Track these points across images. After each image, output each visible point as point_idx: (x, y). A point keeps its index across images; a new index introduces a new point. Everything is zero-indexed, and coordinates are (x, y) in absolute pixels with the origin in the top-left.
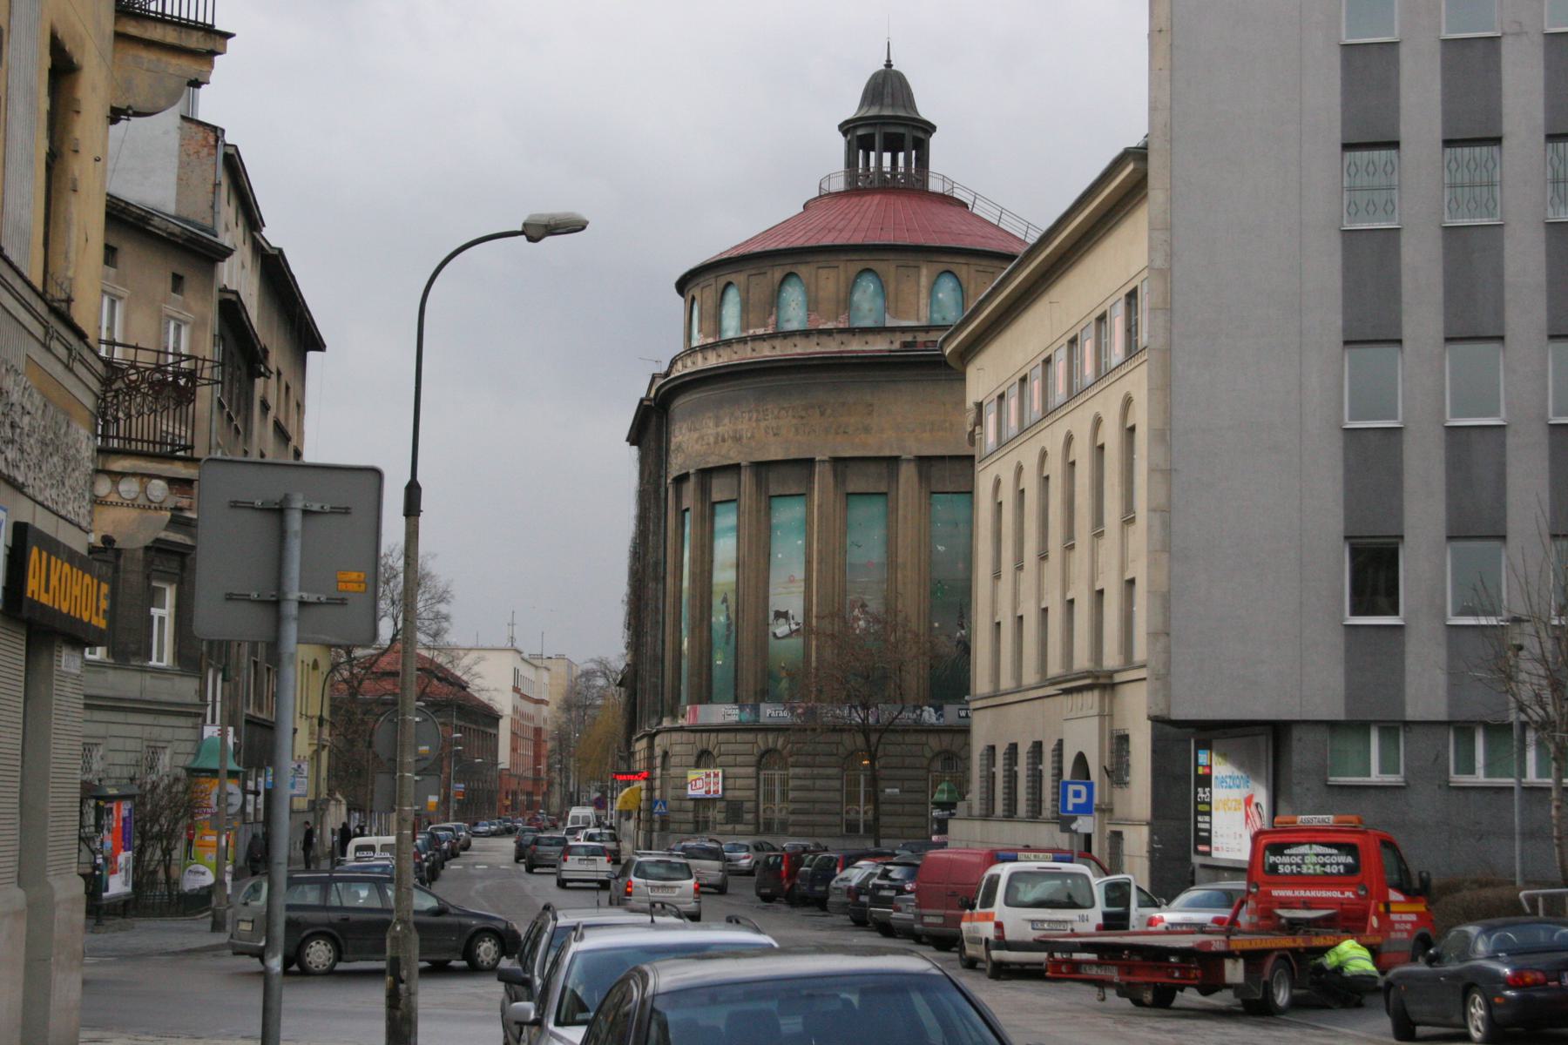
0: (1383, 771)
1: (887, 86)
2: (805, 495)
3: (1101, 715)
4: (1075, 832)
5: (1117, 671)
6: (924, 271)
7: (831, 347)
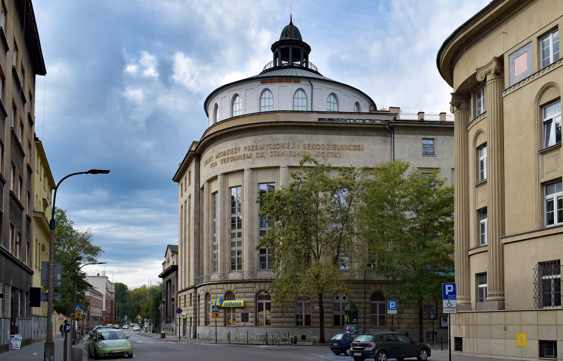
0: (263, 303)
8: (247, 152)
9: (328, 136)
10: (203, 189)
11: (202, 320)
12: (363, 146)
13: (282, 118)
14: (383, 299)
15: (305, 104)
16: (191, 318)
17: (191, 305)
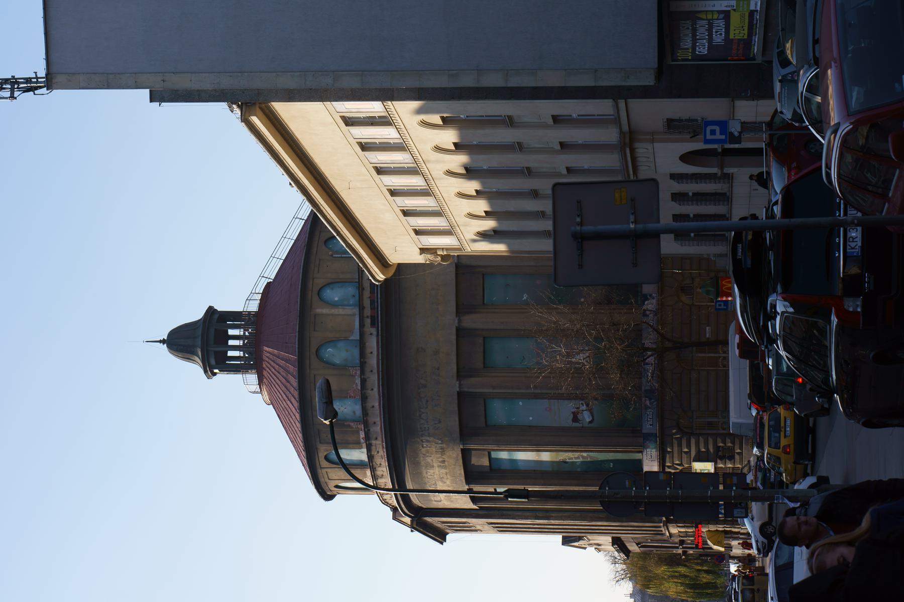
1: (181, 341)
2: (485, 398)
3: (653, 141)
4: (740, 133)
5: (621, 129)
6: (319, 311)
7: (374, 379)
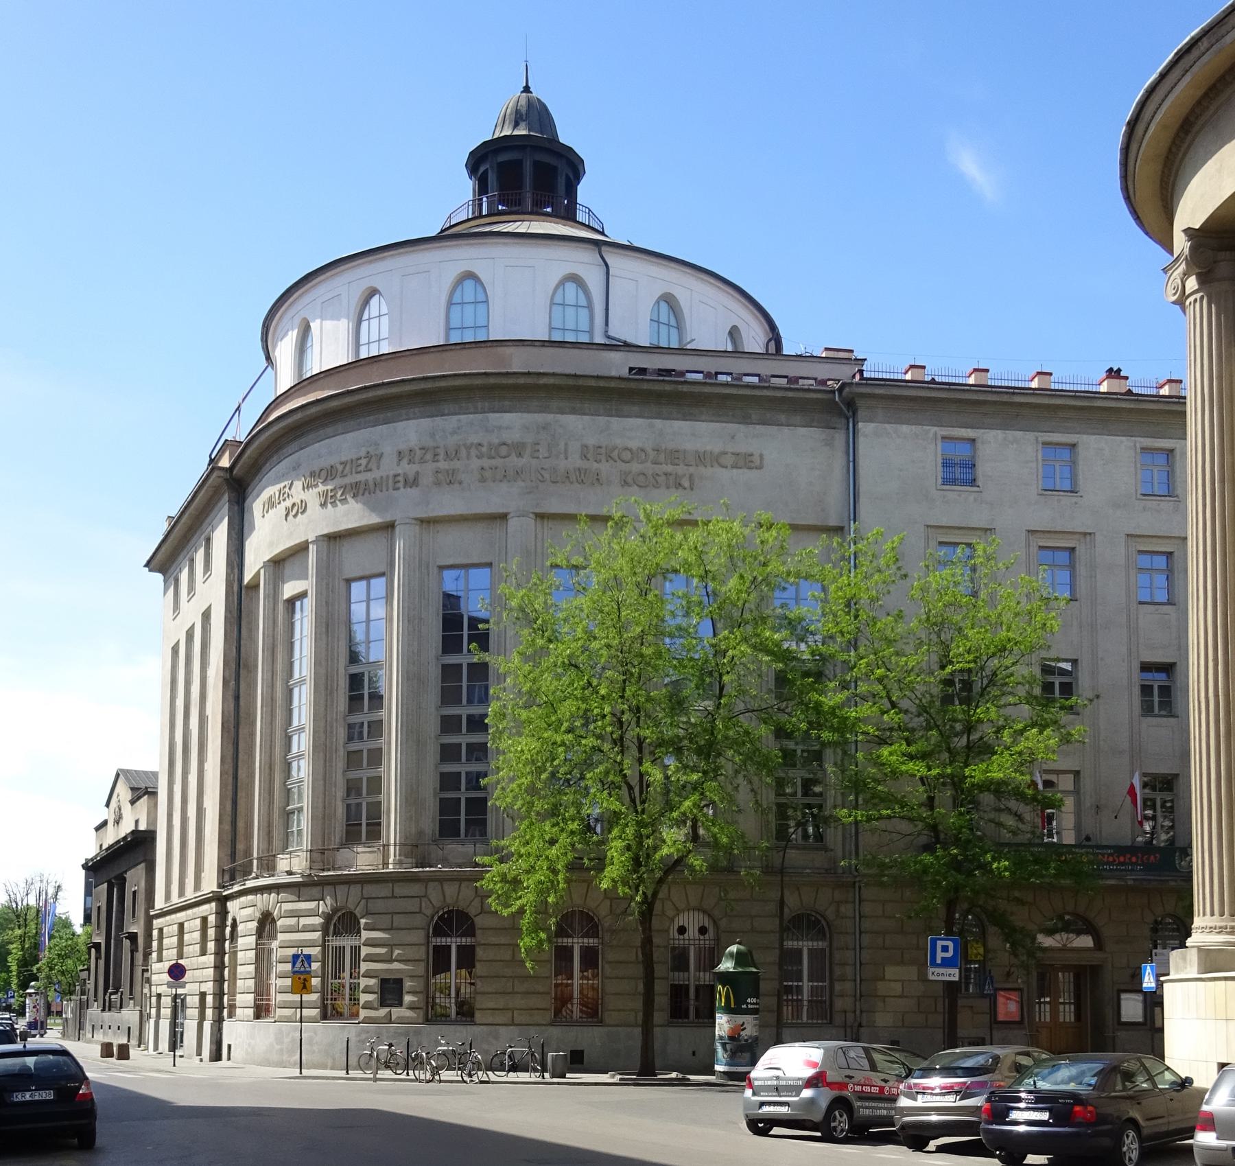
0: (800, 952)
8: (407, 468)
9: (658, 423)
10: (254, 586)
11: (245, 999)
12: (761, 456)
13: (518, 362)
14: (471, 932)
15: (584, 325)
16: (203, 995)
17: (203, 952)
